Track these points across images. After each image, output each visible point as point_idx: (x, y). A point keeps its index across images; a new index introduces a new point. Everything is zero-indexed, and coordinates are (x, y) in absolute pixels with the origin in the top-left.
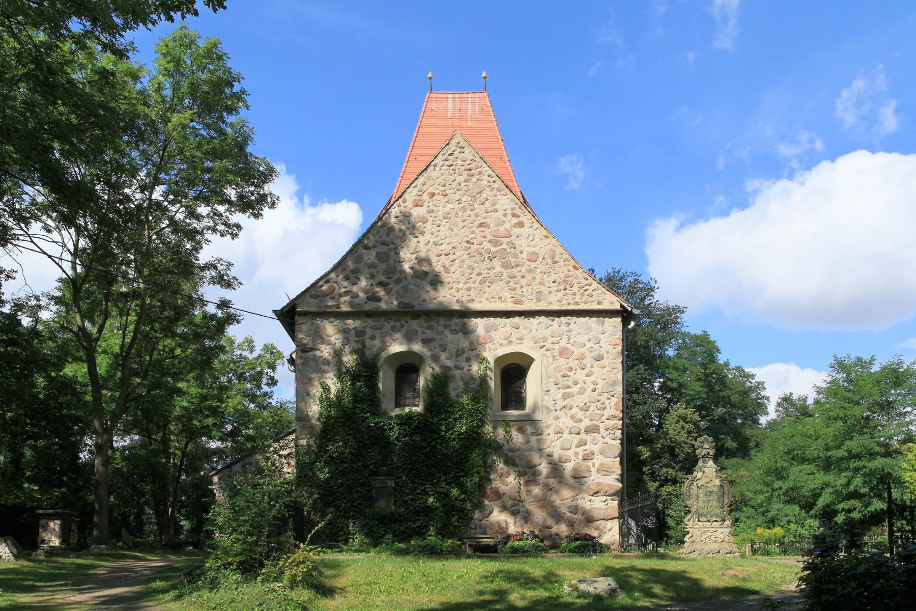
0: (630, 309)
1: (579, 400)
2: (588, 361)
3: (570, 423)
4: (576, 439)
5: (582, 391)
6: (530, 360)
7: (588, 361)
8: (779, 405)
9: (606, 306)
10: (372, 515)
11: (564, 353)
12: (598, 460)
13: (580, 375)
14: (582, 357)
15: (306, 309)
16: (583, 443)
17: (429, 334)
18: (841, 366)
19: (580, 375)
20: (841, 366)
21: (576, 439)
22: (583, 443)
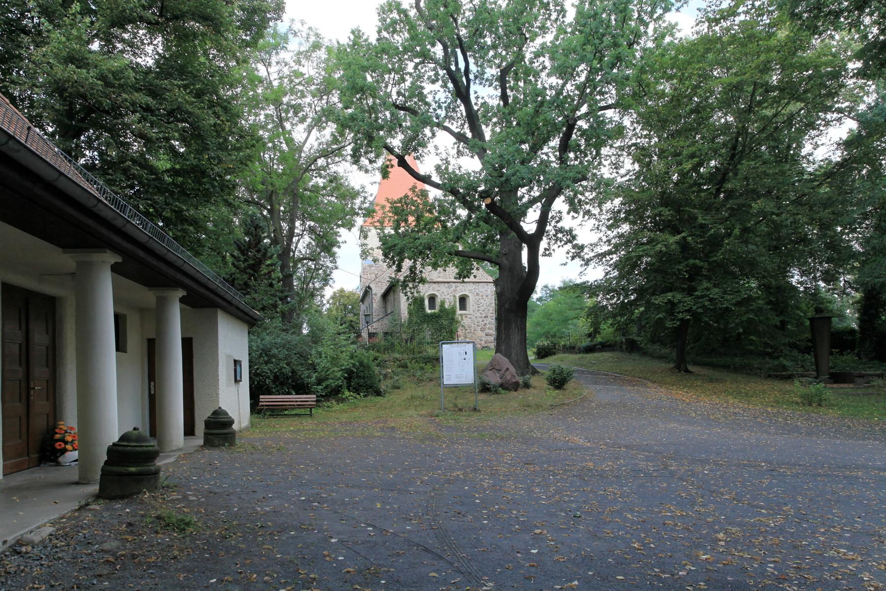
0: (851, 125)
1: (482, 308)
2: (484, 297)
3: (479, 315)
4: (481, 320)
5: (483, 306)
6: (468, 296)
7: (484, 297)
8: (542, 289)
9: (488, 281)
10: (879, 395)
11: (477, 294)
12: (488, 326)
13: (482, 301)
14: (482, 296)
15: (449, 126)
16: (483, 321)
17: (439, 289)
18: (58, 464)
19: (482, 301)
20: (58, 464)
21: (481, 320)
22: (483, 321)
